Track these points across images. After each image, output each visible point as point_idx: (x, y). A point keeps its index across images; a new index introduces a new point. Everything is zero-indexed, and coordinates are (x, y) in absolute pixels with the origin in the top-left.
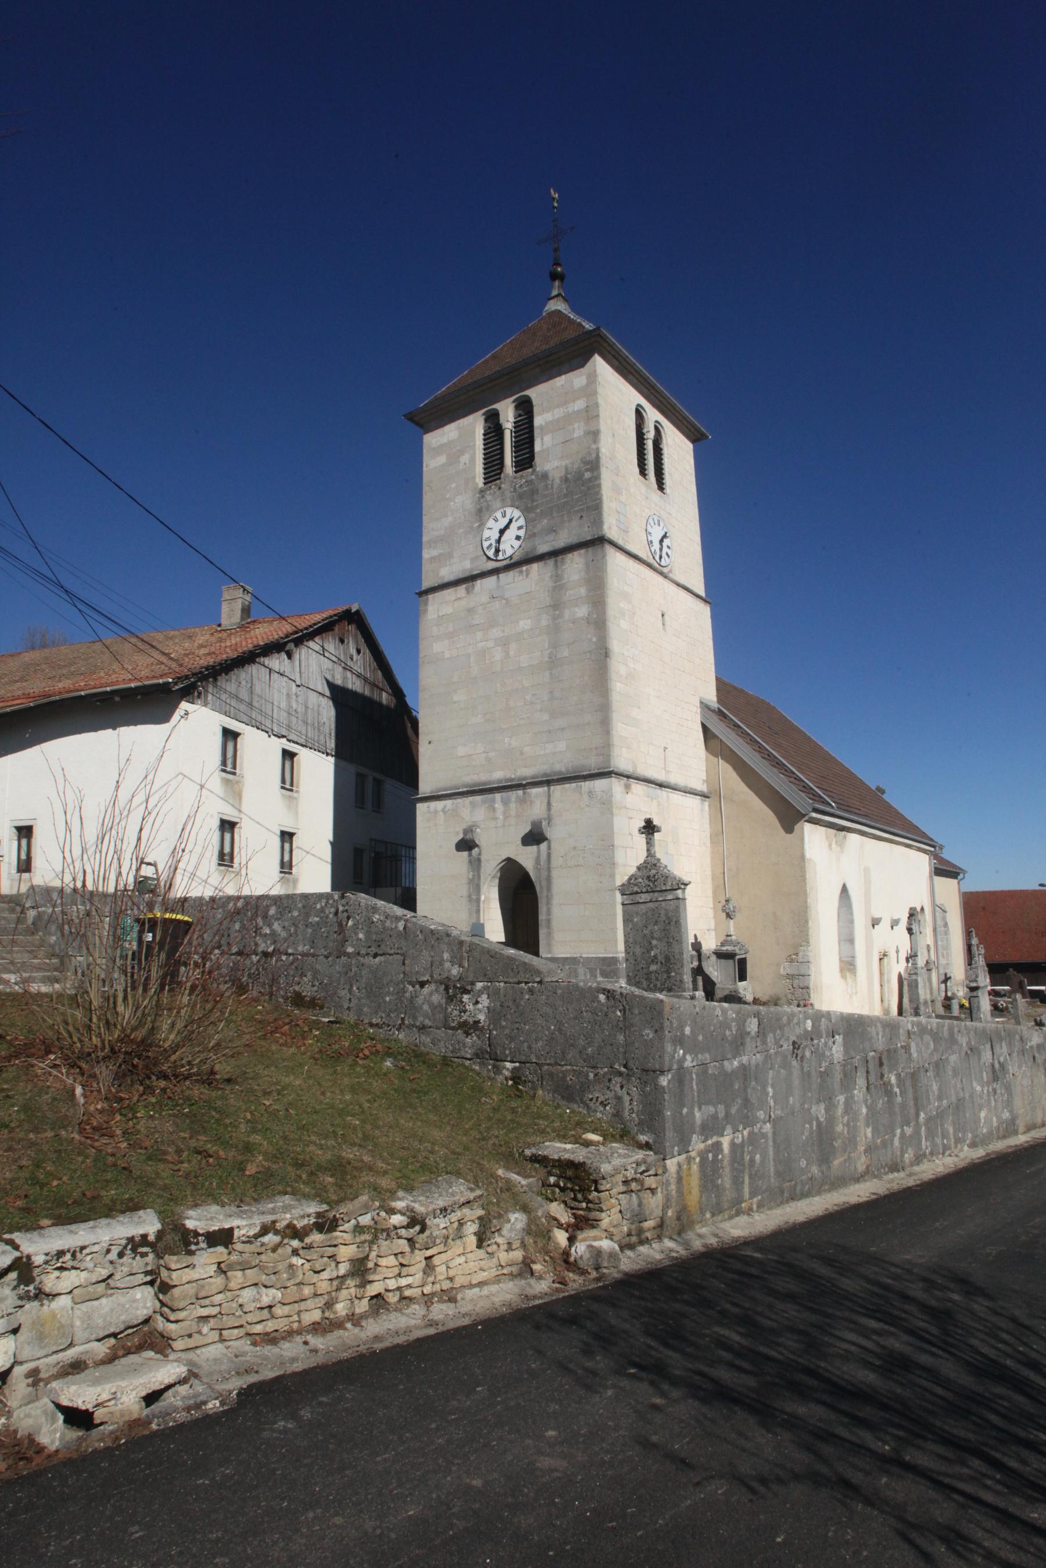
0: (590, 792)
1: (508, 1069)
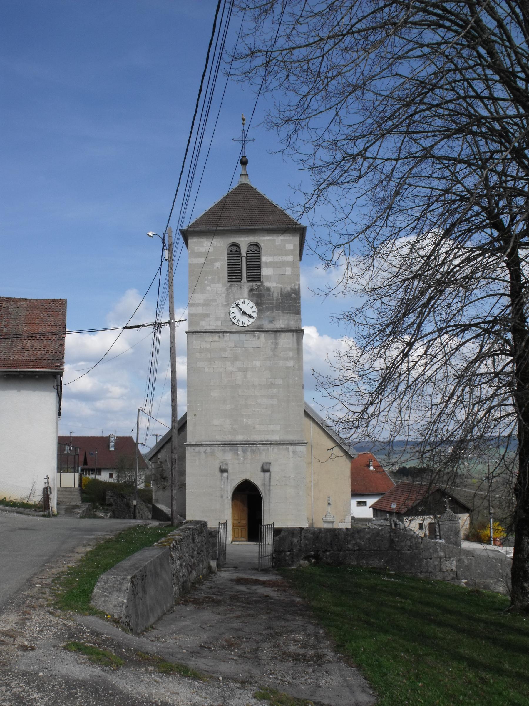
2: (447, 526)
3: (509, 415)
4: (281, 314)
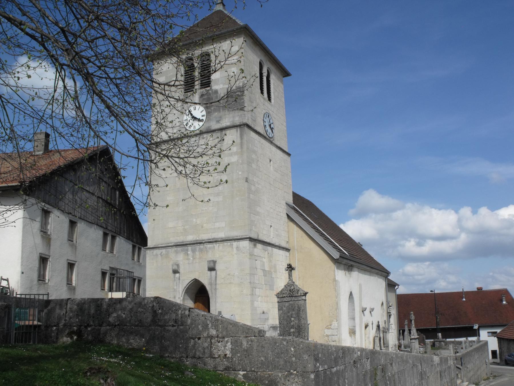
0: (237, 247)
1: (241, 375)
2: (287, 304)
3: (181, 85)
4: (227, 112)
